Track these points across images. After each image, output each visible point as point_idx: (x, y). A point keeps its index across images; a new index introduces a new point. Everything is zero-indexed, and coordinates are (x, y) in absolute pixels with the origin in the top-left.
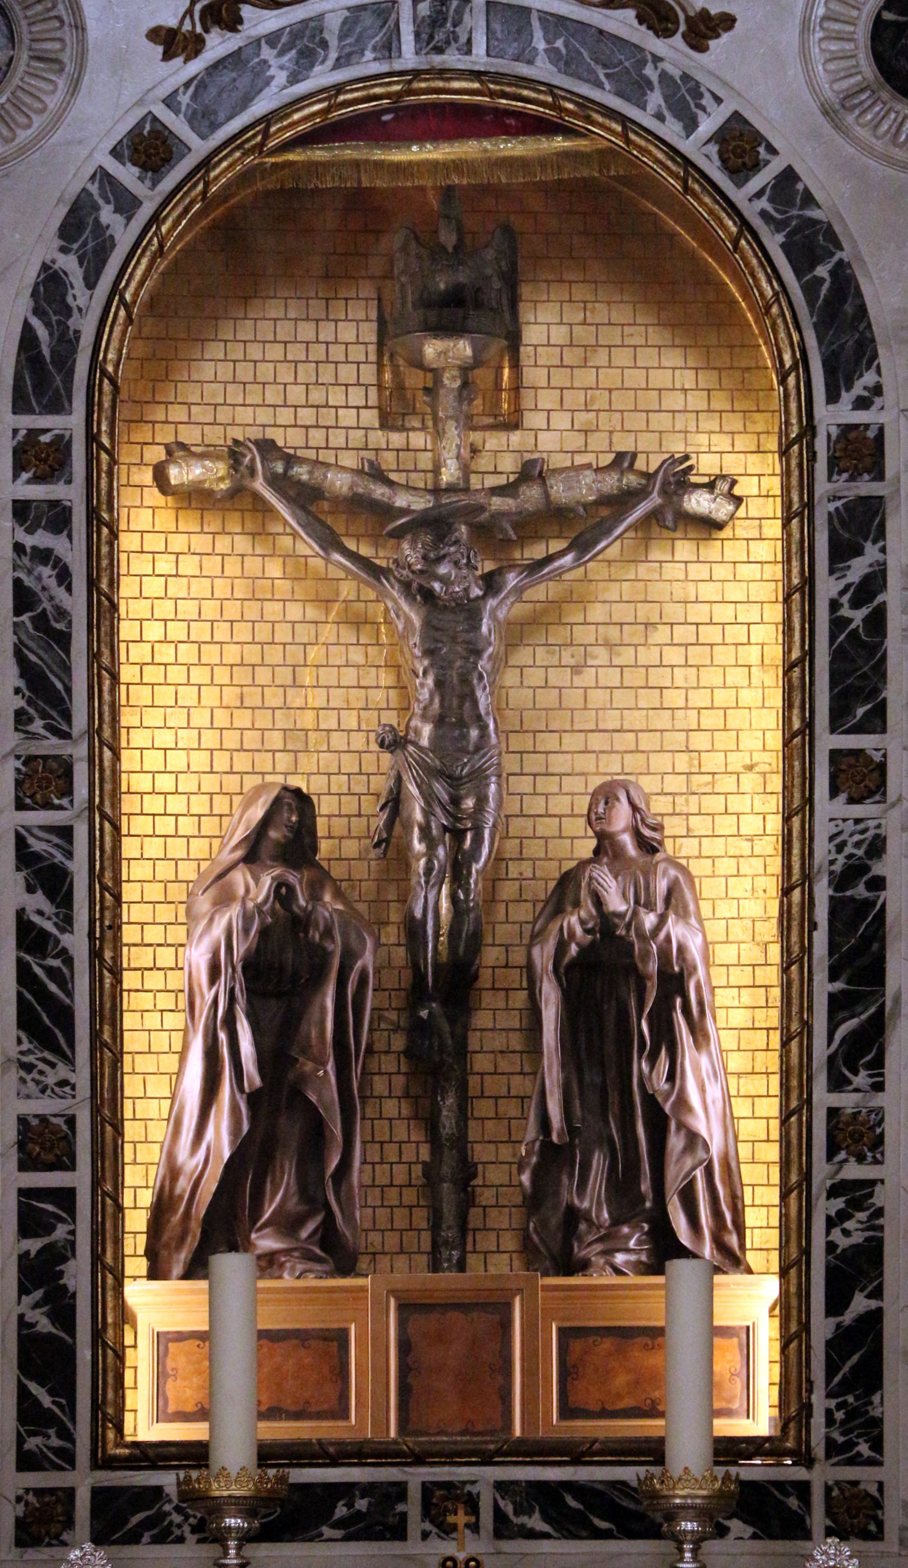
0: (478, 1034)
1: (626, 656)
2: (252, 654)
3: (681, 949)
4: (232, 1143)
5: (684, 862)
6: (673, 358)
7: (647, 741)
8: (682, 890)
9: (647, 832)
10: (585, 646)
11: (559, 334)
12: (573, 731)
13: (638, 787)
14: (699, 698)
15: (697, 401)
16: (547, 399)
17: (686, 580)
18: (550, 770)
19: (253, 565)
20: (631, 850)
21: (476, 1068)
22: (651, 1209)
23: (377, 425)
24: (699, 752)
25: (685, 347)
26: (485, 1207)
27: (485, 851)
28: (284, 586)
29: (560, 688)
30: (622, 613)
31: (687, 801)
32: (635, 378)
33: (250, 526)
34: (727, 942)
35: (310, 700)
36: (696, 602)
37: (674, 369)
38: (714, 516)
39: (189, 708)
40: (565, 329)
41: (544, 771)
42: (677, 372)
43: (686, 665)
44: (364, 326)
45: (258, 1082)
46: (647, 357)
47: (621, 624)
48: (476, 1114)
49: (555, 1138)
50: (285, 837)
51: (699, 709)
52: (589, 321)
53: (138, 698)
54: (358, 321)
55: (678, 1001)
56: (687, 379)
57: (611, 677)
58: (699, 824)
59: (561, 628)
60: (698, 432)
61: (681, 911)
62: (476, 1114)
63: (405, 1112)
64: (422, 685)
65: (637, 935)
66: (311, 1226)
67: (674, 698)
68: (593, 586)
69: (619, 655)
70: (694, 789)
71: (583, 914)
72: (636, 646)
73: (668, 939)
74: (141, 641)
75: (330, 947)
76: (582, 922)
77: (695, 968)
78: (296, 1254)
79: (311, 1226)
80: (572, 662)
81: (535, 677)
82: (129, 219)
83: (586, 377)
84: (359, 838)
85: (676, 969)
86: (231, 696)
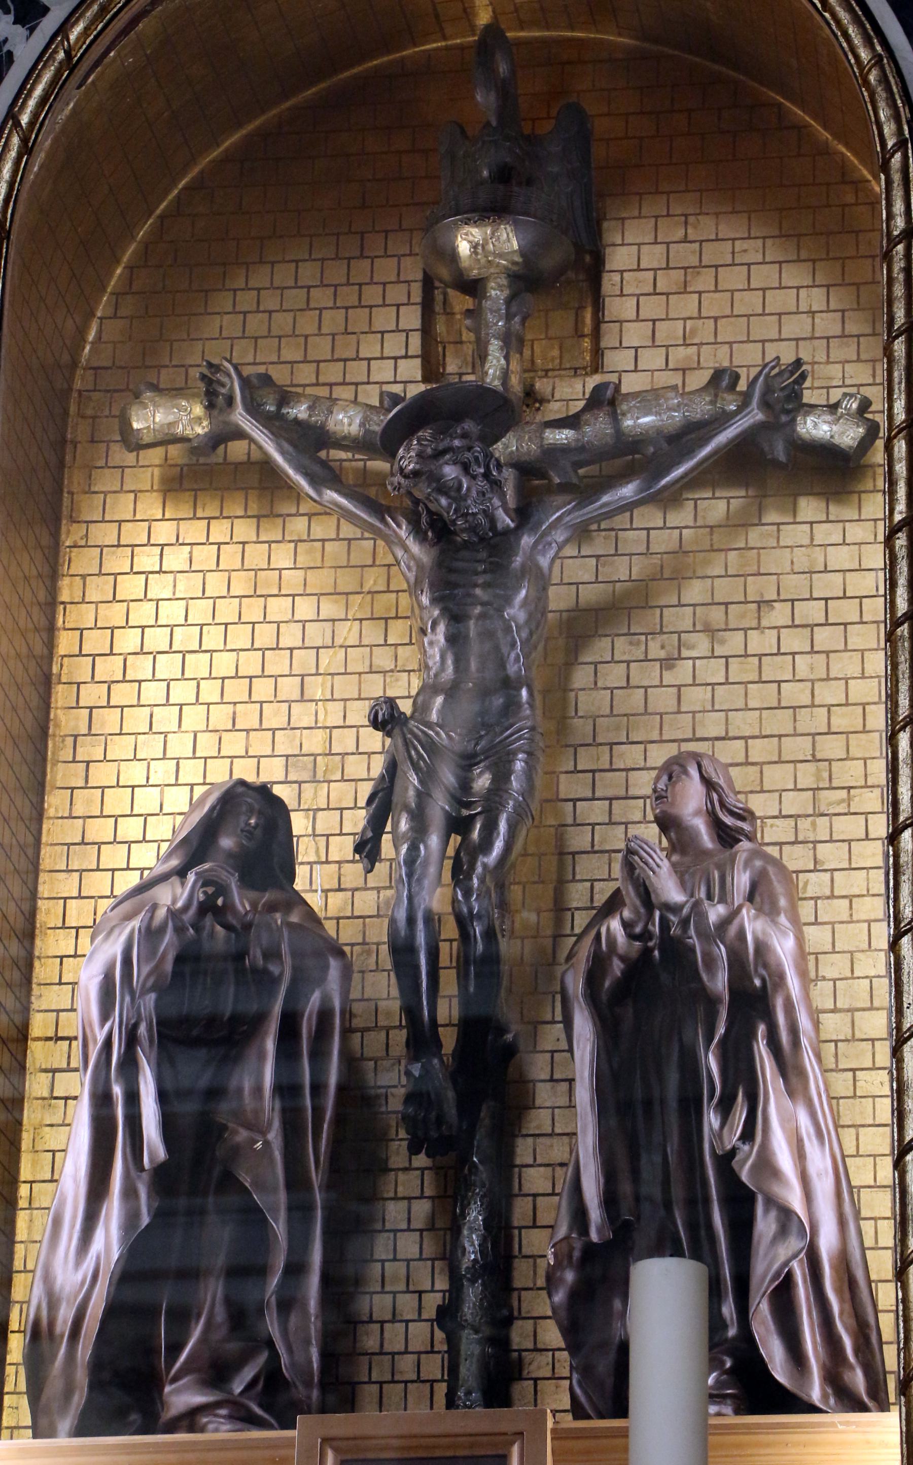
0: (530, 1140)
1: (734, 643)
2: (251, 664)
3: (762, 948)
4: (123, 1239)
5: (773, 851)
6: (795, 275)
7: (760, 750)
8: (770, 882)
9: (728, 820)
10: (679, 633)
11: (653, 256)
12: (662, 741)
13: (712, 758)
14: (830, 694)
15: (828, 324)
16: (635, 334)
17: (812, 545)
18: (631, 792)
19: (256, 555)
20: (707, 840)
21: (528, 1188)
22: (734, 1339)
23: (420, 379)
24: (830, 761)
25: (814, 261)
26: (536, 1380)
27: (499, 845)
28: (293, 579)
29: (646, 688)
30: (725, 589)
31: (814, 824)
32: (750, 302)
33: (254, 509)
34: (871, 1008)
35: (321, 717)
36: (826, 571)
37: (798, 288)
38: (837, 440)
39: (166, 734)
40: (660, 249)
41: (622, 793)
42: (803, 292)
43: (812, 652)
44: (407, 262)
45: (162, 1154)
46: (764, 275)
47: (726, 604)
48: (525, 1251)
49: (594, 1236)
50: (241, 846)
51: (829, 707)
52: (690, 238)
53: (103, 724)
54: (399, 257)
55: (761, 1029)
56: (816, 298)
57: (713, 671)
58: (831, 855)
59: (650, 611)
60: (828, 362)
61: (766, 907)
62: (525, 1251)
63: (428, 1251)
64: (431, 643)
65: (699, 934)
66: (248, 1373)
67: (795, 693)
68: (690, 559)
69: (722, 642)
70: (823, 809)
71: (626, 914)
72: (745, 630)
73: (741, 935)
74: (111, 654)
75: (274, 969)
76: (626, 925)
77: (782, 977)
78: (223, 1412)
79: (248, 1373)
80: (662, 654)
81: (614, 675)
82: (32, 30)
83: (689, 305)
84: (378, 889)
85: (757, 982)
86: (220, 716)
